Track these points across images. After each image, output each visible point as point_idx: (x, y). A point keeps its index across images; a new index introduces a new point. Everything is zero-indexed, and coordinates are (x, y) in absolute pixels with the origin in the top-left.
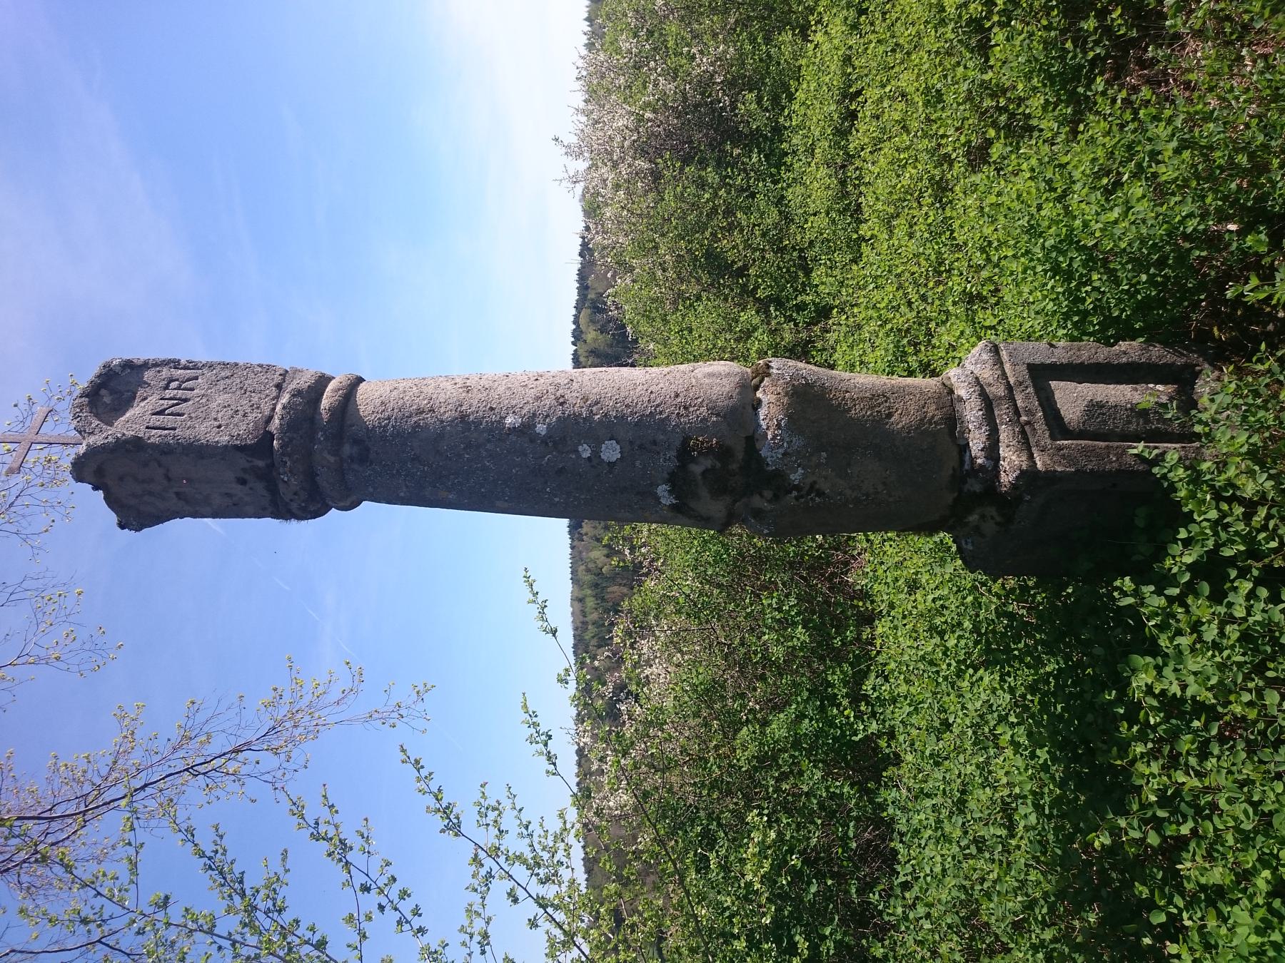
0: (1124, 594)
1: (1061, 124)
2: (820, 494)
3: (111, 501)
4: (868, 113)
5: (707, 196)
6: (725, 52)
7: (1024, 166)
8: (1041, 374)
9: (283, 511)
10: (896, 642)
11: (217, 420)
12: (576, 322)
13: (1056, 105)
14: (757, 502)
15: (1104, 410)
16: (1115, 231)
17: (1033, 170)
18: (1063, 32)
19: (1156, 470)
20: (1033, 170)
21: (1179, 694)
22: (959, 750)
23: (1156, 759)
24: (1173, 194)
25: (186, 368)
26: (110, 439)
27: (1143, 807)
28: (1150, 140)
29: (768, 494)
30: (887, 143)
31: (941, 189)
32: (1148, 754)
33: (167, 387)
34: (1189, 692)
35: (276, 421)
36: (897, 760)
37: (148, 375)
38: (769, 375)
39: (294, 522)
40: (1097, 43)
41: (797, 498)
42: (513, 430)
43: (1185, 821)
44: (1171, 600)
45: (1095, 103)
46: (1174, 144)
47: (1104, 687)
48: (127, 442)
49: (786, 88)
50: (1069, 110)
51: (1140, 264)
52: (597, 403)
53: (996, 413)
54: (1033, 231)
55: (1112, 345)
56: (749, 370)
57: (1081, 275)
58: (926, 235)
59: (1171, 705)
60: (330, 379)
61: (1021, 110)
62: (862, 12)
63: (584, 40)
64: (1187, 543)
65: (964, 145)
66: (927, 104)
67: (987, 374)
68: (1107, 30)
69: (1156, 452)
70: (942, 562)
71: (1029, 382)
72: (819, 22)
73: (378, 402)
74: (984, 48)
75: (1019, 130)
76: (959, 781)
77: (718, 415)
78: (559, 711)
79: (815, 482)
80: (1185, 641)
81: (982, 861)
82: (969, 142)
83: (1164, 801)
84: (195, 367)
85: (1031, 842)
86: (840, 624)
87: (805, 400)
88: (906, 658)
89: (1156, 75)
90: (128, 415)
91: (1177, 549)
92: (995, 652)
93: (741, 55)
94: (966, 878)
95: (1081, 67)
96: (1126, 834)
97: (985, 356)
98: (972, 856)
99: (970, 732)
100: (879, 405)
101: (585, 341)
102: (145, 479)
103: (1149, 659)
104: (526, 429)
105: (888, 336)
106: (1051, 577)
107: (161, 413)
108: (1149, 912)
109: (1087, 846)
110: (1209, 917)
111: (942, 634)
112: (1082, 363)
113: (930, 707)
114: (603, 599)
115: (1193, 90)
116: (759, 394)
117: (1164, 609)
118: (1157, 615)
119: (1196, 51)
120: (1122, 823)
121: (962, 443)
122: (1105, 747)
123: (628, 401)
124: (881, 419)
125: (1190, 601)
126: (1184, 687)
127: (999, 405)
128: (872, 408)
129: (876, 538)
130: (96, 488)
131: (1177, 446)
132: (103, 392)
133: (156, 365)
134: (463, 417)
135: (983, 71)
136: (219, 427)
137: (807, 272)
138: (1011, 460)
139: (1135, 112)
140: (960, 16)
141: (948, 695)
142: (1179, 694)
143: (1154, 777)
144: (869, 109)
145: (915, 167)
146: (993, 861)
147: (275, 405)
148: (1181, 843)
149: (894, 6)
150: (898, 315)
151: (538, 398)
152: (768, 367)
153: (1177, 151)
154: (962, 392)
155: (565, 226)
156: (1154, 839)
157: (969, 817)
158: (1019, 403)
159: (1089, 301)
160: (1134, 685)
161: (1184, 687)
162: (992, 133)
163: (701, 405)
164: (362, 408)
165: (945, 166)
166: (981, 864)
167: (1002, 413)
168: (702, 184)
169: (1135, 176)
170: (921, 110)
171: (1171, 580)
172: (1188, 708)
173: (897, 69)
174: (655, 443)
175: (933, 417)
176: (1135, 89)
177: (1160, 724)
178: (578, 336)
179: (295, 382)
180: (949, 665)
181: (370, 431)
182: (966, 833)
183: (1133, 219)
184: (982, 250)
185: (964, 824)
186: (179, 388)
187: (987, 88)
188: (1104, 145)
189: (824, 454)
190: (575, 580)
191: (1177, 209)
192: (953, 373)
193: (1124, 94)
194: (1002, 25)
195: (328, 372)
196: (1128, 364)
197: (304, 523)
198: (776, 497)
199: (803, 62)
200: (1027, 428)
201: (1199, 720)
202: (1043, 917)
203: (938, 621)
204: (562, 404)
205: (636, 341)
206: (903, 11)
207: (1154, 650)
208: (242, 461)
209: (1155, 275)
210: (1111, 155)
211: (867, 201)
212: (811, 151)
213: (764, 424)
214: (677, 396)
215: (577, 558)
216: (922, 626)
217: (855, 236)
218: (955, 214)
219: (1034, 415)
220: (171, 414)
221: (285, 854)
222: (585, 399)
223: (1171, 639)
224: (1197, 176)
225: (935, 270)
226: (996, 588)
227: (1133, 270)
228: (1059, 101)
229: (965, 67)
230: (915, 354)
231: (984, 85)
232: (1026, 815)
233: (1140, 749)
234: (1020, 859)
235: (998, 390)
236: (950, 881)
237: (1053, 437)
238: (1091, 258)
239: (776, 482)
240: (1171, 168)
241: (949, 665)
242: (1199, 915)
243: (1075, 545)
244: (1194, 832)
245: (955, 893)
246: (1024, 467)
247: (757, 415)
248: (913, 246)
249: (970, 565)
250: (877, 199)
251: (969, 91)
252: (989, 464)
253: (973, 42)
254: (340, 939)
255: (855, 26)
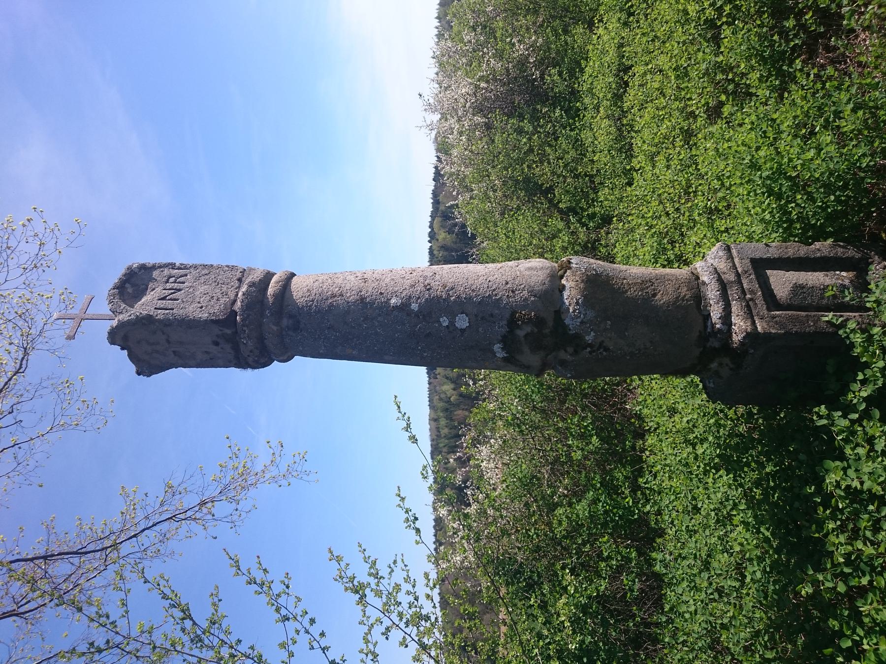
0: (821, 417)
1: (772, 91)
2: (606, 349)
3: (131, 357)
4: (636, 83)
5: (524, 140)
6: (536, 41)
7: (747, 121)
8: (760, 266)
9: (242, 364)
10: (663, 451)
11: (200, 303)
12: (431, 226)
13: (768, 77)
14: (562, 355)
15: (805, 290)
16: (811, 166)
17: (753, 123)
18: (771, 29)
19: (841, 332)
20: (753, 123)
21: (859, 487)
22: (706, 527)
23: (843, 532)
24: (851, 140)
25: (179, 268)
26: (133, 317)
27: (834, 565)
28: (834, 103)
29: (570, 350)
30: (650, 104)
31: (688, 135)
32: (837, 529)
33: (167, 282)
34: (865, 487)
35: (239, 303)
36: (661, 533)
37: (155, 274)
38: (570, 268)
39: (249, 370)
40: (795, 36)
41: (590, 353)
42: (396, 307)
43: (864, 575)
44: (853, 422)
45: (795, 77)
46: (851, 106)
47: (807, 483)
48: (143, 318)
49: (578, 64)
50: (777, 82)
51: (829, 188)
52: (452, 289)
53: (729, 293)
54: (754, 166)
55: (810, 244)
56: (556, 265)
57: (788, 197)
58: (679, 167)
59: (852, 494)
60: (274, 274)
61: (743, 81)
62: (631, 14)
63: (436, 32)
64: (864, 382)
65: (704, 106)
66: (677, 77)
67: (722, 266)
68: (803, 27)
69: (841, 319)
70: (694, 396)
71: (751, 271)
72: (601, 21)
73: (305, 289)
74: (716, 40)
75: (742, 95)
76: (706, 548)
77: (535, 296)
78: (423, 500)
79: (603, 341)
80: (861, 451)
81: (722, 604)
82: (708, 103)
83: (848, 562)
84: (185, 268)
85: (758, 591)
86: (622, 441)
87: (595, 284)
88: (668, 462)
89: (838, 57)
90: (143, 300)
91: (856, 387)
92: (730, 461)
93: (547, 43)
94: (711, 615)
95: (785, 52)
96: (823, 585)
97: (721, 253)
98: (714, 600)
99: (713, 514)
100: (647, 288)
101: (437, 240)
102: (153, 344)
103: (838, 463)
104: (404, 307)
105: (653, 237)
106: (768, 405)
107: (164, 299)
108: (839, 639)
109: (797, 594)
110: (880, 643)
111: (694, 446)
112: (789, 258)
113: (685, 496)
114: (451, 420)
115: (864, 67)
116: (564, 282)
117: (847, 428)
118: (844, 432)
119: (865, 40)
120: (820, 577)
121: (706, 313)
122: (807, 524)
123: (474, 287)
124: (649, 298)
125: (865, 423)
126: (862, 483)
127: (731, 287)
128: (642, 290)
129: (646, 378)
130: (123, 349)
131: (856, 314)
132: (127, 285)
133: (160, 267)
134: (362, 299)
135: (716, 55)
136: (201, 307)
137: (595, 191)
138: (740, 325)
139: (824, 83)
140: (699, 18)
141: (698, 488)
142: (859, 487)
143: (842, 545)
144: (637, 81)
145: (670, 121)
146: (730, 604)
147: (237, 293)
148: (862, 592)
149: (653, 10)
150: (660, 223)
151: (412, 286)
152: (570, 263)
153: (854, 111)
154: (705, 278)
155: (425, 158)
156: (841, 588)
157: (713, 573)
158: (745, 286)
159: (794, 213)
160: (828, 481)
161: (862, 483)
162: (723, 98)
163: (523, 289)
164: (295, 294)
165: (691, 120)
166: (721, 606)
167: (733, 293)
168: (520, 131)
169: (825, 127)
170: (673, 82)
171: (852, 408)
172: (865, 496)
173: (656, 53)
174: (492, 315)
175: (685, 296)
176: (823, 67)
177: (846, 508)
178: (432, 236)
179: (251, 277)
180: (699, 467)
181: (300, 309)
182: (711, 584)
183: (822, 158)
184: (719, 179)
185: (709, 578)
186: (175, 282)
187: (719, 67)
188: (802, 107)
189: (609, 322)
190: (432, 406)
191: (854, 151)
192: (699, 265)
193: (816, 70)
194: (729, 24)
195: (272, 270)
196: (821, 258)
197: (256, 371)
198: (576, 352)
199: (590, 47)
200: (750, 303)
201: (873, 505)
202: (765, 642)
203: (691, 436)
204: (428, 290)
205: (474, 237)
206: (659, 14)
207: (842, 457)
208: (216, 330)
209: (840, 196)
210: (807, 115)
211: (637, 142)
212: (597, 108)
213: (567, 302)
214: (507, 283)
215: (433, 391)
216: (680, 439)
217: (628, 167)
218: (698, 153)
219: (755, 294)
220: (170, 299)
221: (348, 565)
222: (444, 286)
223: (853, 449)
224: (868, 128)
225: (685, 190)
226: (731, 413)
227: (824, 193)
228: (770, 75)
229: (704, 52)
230: (672, 249)
231: (718, 66)
232: (754, 571)
233: (831, 525)
234: (748, 603)
235: (730, 277)
236: (700, 618)
237: (769, 309)
238: (796, 185)
239: (575, 341)
240: (849, 123)
241: (699, 467)
242: (875, 641)
243: (782, 384)
244: (871, 582)
245: (704, 625)
246: (749, 330)
247: (562, 295)
248: (669, 175)
249: (713, 397)
250: (644, 142)
251: (707, 69)
252: (725, 328)
253: (709, 35)
254: (274, 656)
255: (626, 24)
